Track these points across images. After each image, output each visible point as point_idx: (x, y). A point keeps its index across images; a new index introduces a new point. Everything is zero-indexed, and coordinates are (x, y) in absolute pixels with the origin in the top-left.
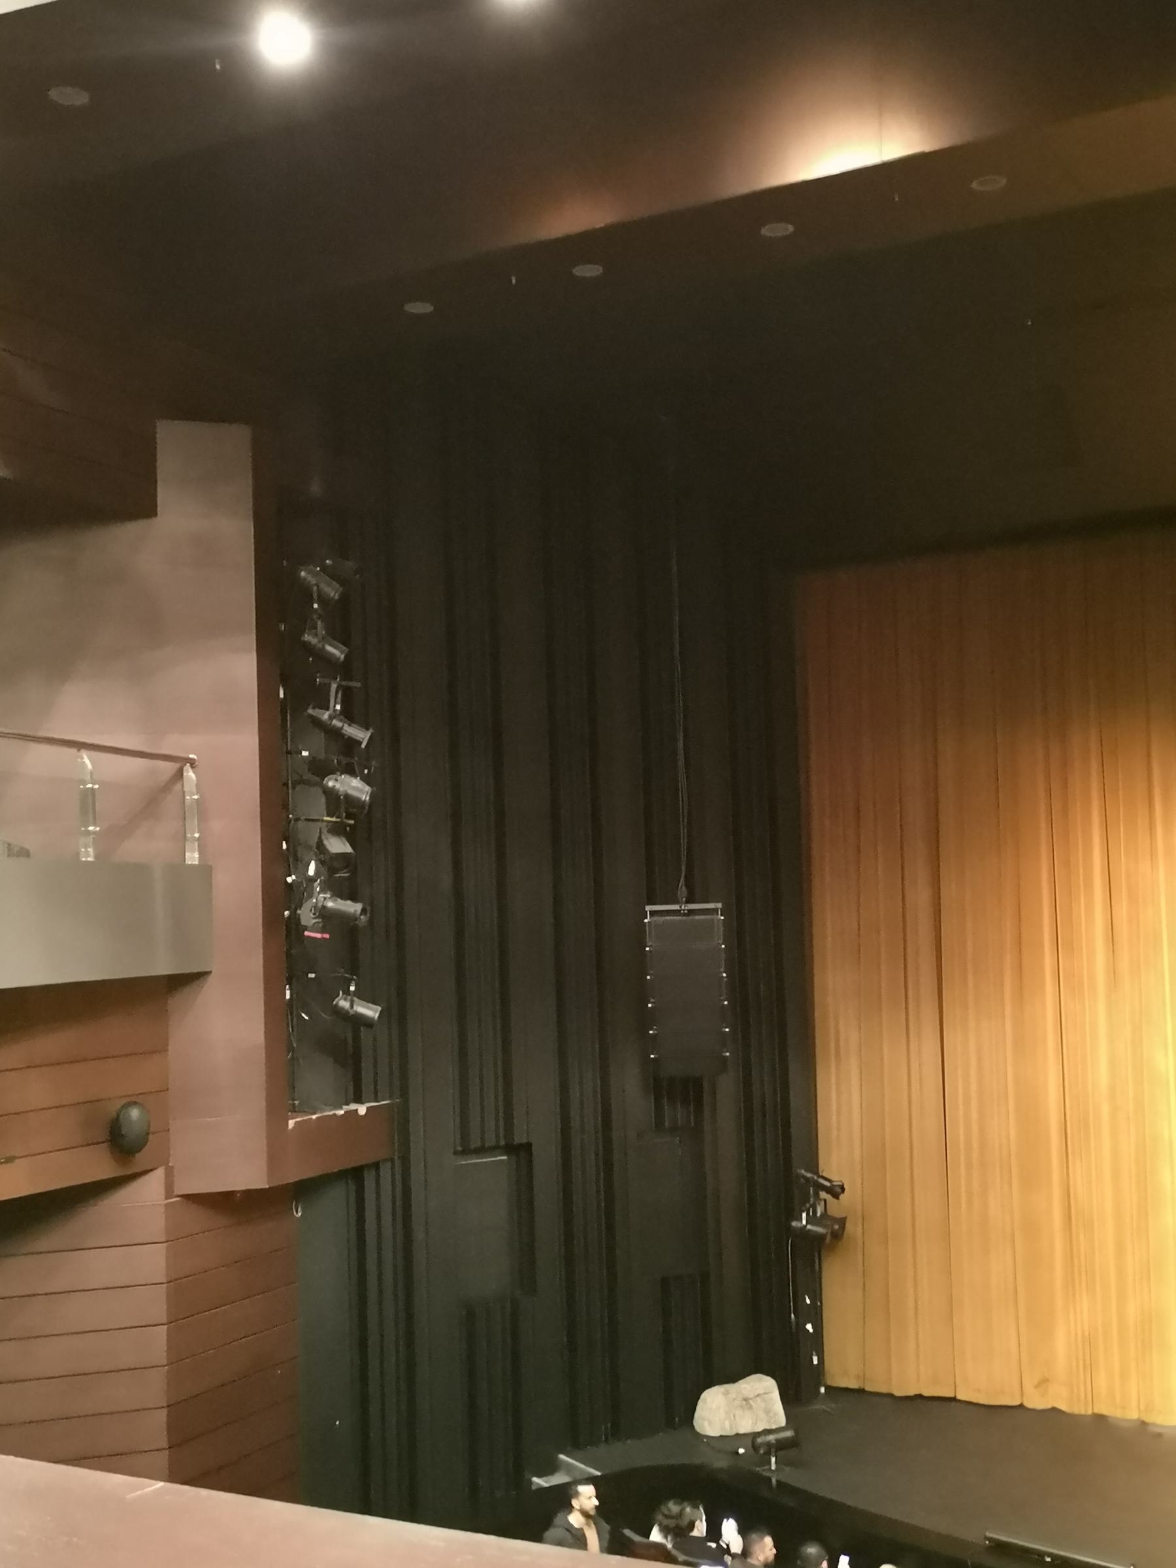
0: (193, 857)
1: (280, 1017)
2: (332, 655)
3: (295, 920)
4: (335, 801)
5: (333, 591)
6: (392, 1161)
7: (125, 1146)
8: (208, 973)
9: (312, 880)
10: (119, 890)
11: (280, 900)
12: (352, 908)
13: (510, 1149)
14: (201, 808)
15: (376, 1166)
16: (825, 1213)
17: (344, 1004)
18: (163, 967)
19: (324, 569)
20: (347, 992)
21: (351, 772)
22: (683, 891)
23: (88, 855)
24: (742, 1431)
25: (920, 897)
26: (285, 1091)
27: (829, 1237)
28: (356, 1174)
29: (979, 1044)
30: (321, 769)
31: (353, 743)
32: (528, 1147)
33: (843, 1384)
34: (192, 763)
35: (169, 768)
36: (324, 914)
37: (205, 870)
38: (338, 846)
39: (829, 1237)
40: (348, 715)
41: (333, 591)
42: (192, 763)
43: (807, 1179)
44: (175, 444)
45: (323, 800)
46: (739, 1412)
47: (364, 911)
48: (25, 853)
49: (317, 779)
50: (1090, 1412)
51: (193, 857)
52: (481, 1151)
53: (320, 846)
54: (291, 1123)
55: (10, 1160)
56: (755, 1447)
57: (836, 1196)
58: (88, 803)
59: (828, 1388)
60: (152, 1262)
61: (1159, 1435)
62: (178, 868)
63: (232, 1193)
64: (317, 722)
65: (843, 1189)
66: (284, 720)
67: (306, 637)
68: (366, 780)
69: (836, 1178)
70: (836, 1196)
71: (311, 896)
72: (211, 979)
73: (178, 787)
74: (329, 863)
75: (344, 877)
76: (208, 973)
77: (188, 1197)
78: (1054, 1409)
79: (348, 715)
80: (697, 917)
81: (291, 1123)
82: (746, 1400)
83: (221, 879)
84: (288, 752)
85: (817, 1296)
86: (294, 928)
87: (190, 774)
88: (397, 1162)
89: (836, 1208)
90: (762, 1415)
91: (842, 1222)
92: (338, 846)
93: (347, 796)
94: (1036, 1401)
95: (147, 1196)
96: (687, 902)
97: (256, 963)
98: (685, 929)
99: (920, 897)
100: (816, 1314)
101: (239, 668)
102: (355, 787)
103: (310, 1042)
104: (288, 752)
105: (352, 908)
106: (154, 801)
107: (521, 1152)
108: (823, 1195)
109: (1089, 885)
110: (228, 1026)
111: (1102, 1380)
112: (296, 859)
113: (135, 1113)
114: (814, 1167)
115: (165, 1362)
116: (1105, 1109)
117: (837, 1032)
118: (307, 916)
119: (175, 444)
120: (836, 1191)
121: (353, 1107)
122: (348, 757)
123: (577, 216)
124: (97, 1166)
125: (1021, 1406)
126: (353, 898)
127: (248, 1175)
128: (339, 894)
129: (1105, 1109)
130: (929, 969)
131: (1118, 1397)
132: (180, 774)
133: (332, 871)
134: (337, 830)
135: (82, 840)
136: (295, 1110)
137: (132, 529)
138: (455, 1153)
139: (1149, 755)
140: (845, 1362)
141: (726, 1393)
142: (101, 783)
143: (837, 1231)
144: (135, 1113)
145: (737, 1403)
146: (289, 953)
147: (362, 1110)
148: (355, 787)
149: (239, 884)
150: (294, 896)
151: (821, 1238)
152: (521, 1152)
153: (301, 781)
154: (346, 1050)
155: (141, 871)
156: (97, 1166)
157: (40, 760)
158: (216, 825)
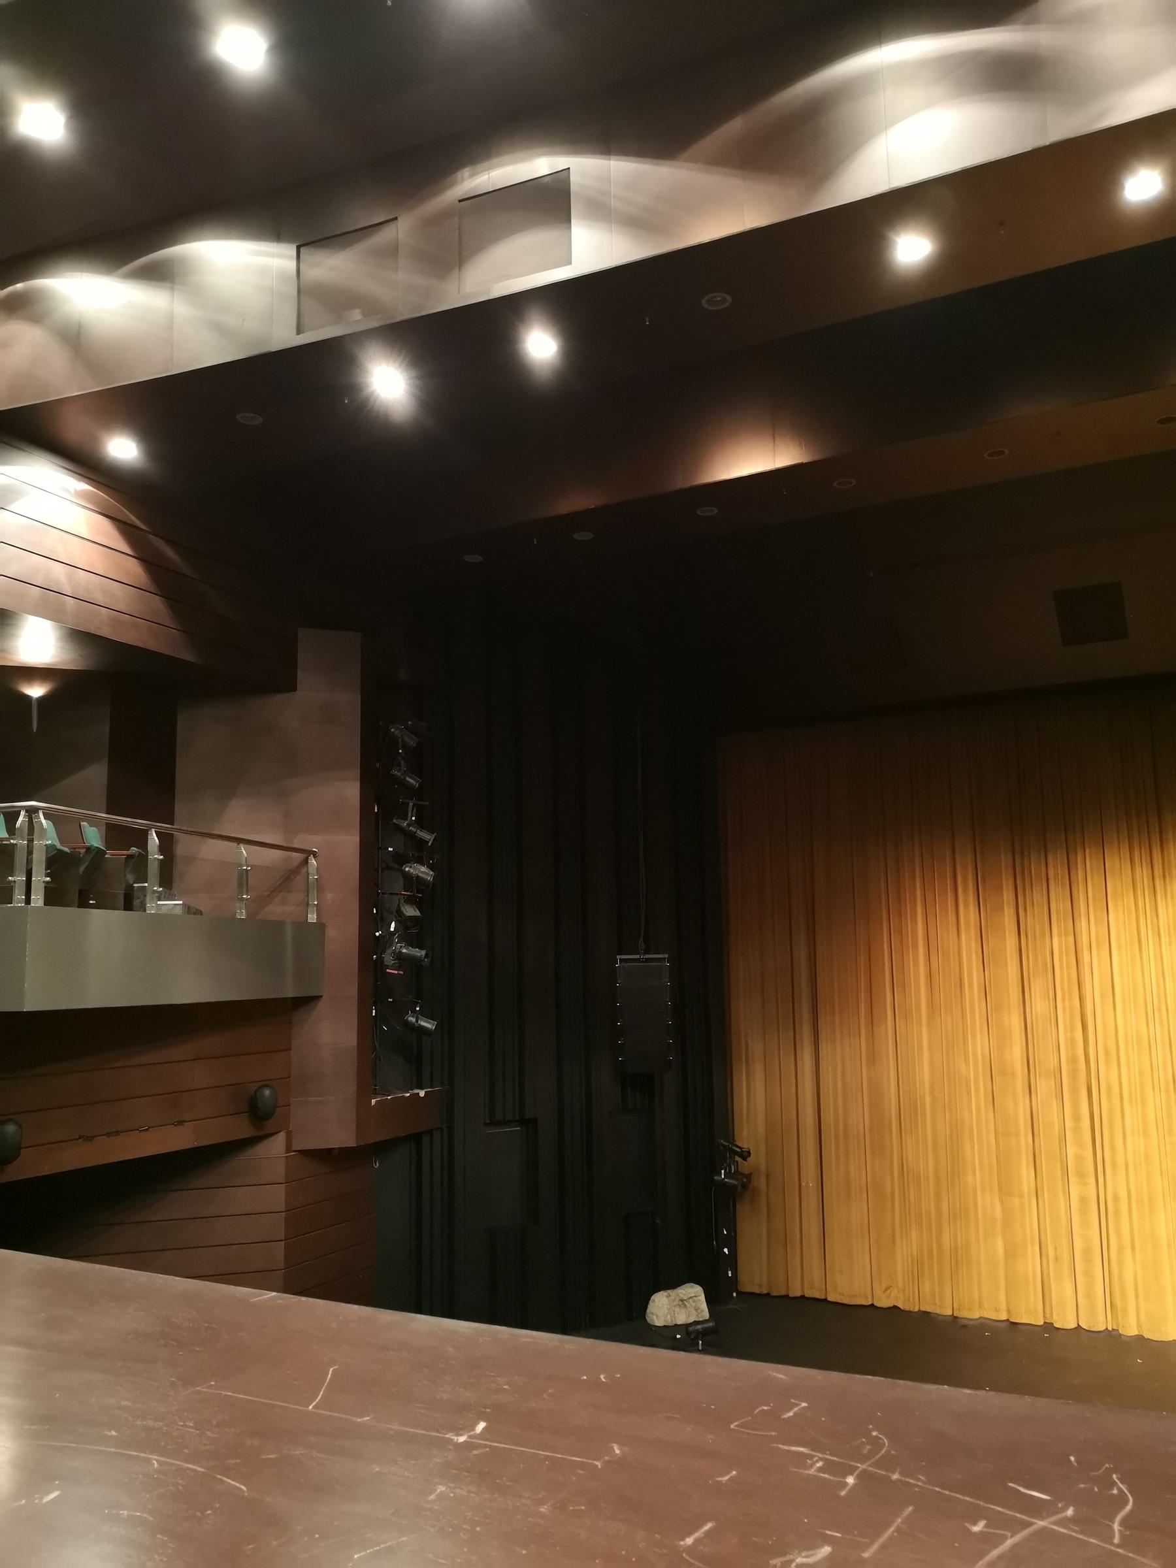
0: (312, 918)
1: (367, 1028)
2: (48, 1493)
3: (380, 960)
4: (410, 880)
5: (412, 742)
6: (441, 1129)
7: (261, 1117)
8: (318, 998)
9: (393, 934)
10: (262, 939)
11: (370, 947)
12: (420, 953)
13: (523, 1122)
14: (320, 886)
15: (430, 1132)
16: (737, 1171)
17: (412, 1019)
18: (290, 991)
19: (407, 728)
20: (414, 1011)
21: (422, 864)
22: (642, 945)
23: (242, 915)
24: (679, 1323)
25: (802, 952)
26: (370, 1076)
27: (739, 1188)
28: (415, 1139)
29: (843, 1057)
30: (401, 859)
31: (423, 842)
32: (534, 1121)
33: (750, 1289)
34: (315, 854)
35: (302, 856)
36: (399, 957)
37: (321, 926)
38: (410, 911)
39: (739, 1188)
40: (420, 823)
41: (412, 742)
42: (315, 854)
43: (724, 1146)
44: (310, 645)
45: (402, 882)
46: (677, 1309)
47: (427, 956)
48: (200, 912)
49: (396, 866)
50: (916, 1310)
51: (312, 918)
52: (505, 1123)
53: (399, 912)
54: (373, 1101)
55: (181, 1123)
56: (688, 1334)
57: (745, 1159)
58: (243, 879)
59: (739, 1293)
60: (276, 1197)
61: (965, 1326)
62: (302, 926)
63: (330, 1150)
64: (399, 829)
65: (749, 1153)
66: (377, 828)
67: (395, 772)
68: (431, 867)
69: (745, 1146)
70: (745, 1159)
71: (391, 945)
72: (322, 1007)
73: (304, 870)
74: (403, 921)
75: (412, 932)
76: (318, 998)
77: (304, 1153)
78: (895, 1307)
79: (420, 823)
80: (1062, 1200)
81: (373, 1101)
82: (682, 1300)
83: (331, 932)
84: (379, 848)
85: (733, 1229)
86: (380, 965)
87: (313, 861)
88: (445, 1131)
89: (745, 1166)
90: (694, 1312)
91: (749, 1176)
92: (410, 911)
93: (418, 877)
94: (884, 1302)
95: (276, 1146)
96: (645, 953)
97: (353, 991)
98: (643, 971)
99: (802, 952)
100: (732, 1242)
101: (350, 791)
102: (422, 871)
103: (387, 1046)
104: (379, 848)
105: (420, 953)
106: (288, 879)
107: (529, 1124)
108: (737, 1158)
109: (915, 947)
110: (332, 1033)
111: (927, 1287)
112: (382, 920)
113: (267, 1092)
114: (732, 1140)
115: (282, 1266)
116: (928, 1099)
117: (747, 1044)
118: (388, 959)
119: (310, 645)
120: (745, 1155)
121: (416, 1091)
122: (420, 852)
123: (575, 501)
124: (241, 1129)
125: (872, 1305)
126: (421, 948)
127: (341, 1136)
128: (410, 944)
129: (928, 1099)
130: (809, 1005)
131: (941, 1302)
132: (306, 861)
133: (407, 928)
134: (410, 901)
135: (238, 905)
136: (376, 1093)
137: (280, 698)
138: (485, 1124)
139: (954, 859)
140: (754, 1274)
141: (669, 1296)
142: (252, 866)
143: (745, 1182)
144: (267, 1092)
145: (677, 1302)
146: (377, 987)
147: (422, 1094)
148: (422, 871)
149: (342, 936)
150: (379, 945)
151: (734, 1187)
152: (529, 1124)
153: (389, 868)
154: (412, 1054)
155: (277, 926)
156: (241, 1129)
157: (212, 850)
158: (329, 896)
